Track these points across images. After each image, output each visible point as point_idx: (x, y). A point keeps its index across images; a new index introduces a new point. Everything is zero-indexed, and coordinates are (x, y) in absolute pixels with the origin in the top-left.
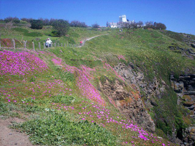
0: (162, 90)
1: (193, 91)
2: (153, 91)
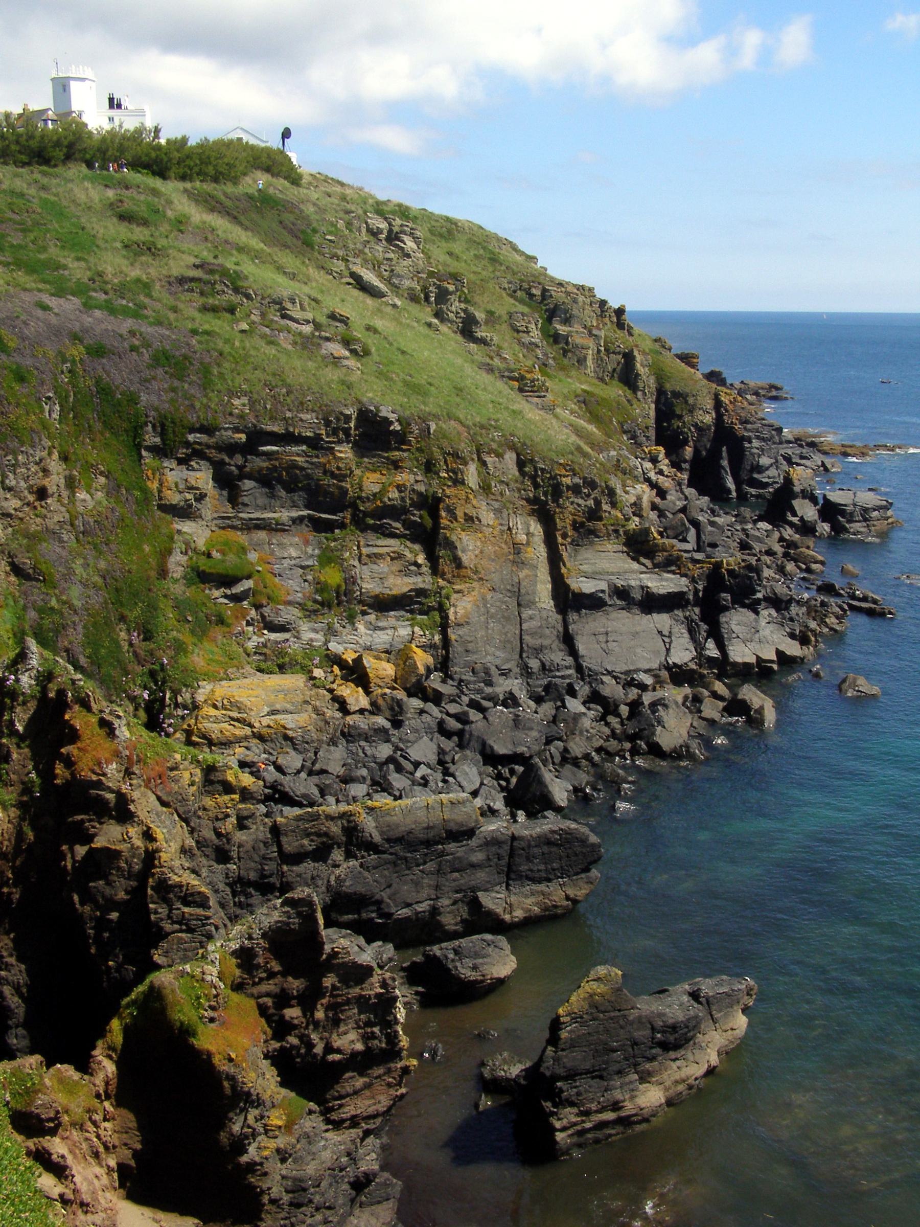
0: (84, 500)
1: (264, 508)
2: (28, 504)
